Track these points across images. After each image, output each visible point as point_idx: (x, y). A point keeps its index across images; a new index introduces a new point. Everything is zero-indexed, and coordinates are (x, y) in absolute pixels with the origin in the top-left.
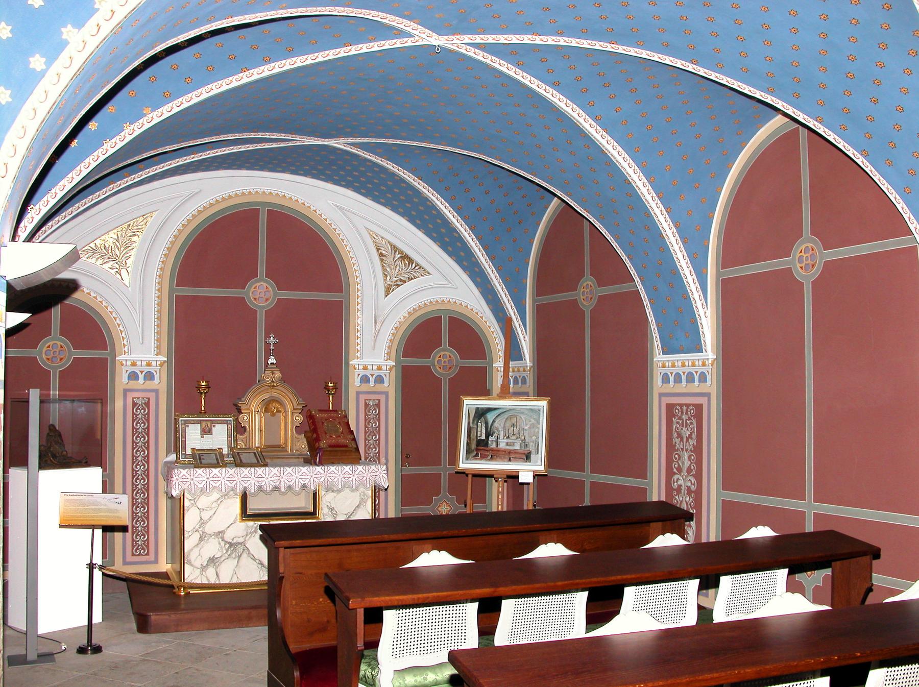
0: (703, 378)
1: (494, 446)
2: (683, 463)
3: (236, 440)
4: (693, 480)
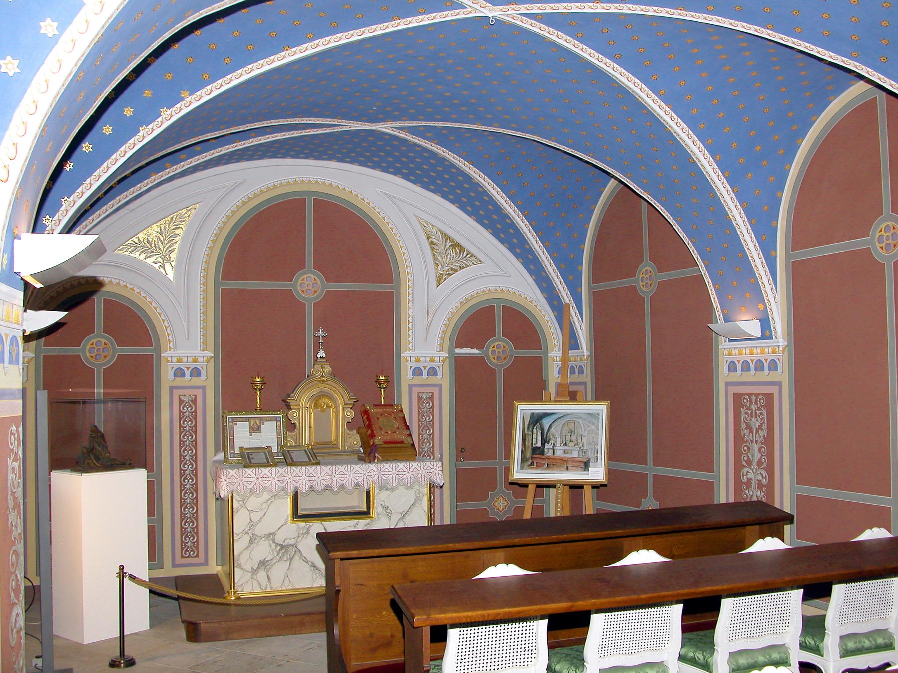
0: (773, 366)
1: (550, 454)
2: (753, 456)
3: (286, 438)
4: (764, 473)
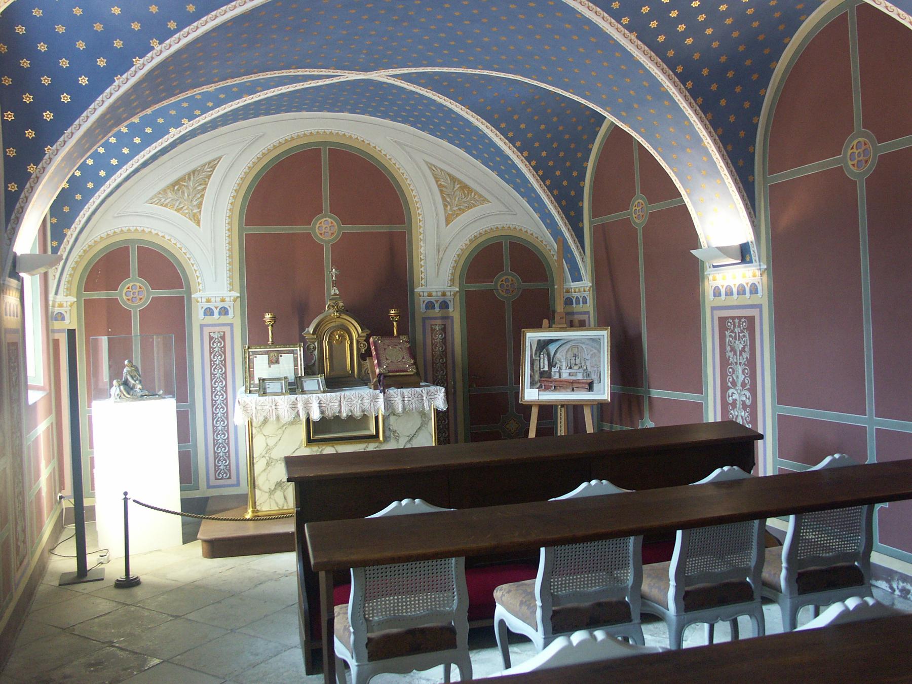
2: (737, 377)
4: (748, 394)
